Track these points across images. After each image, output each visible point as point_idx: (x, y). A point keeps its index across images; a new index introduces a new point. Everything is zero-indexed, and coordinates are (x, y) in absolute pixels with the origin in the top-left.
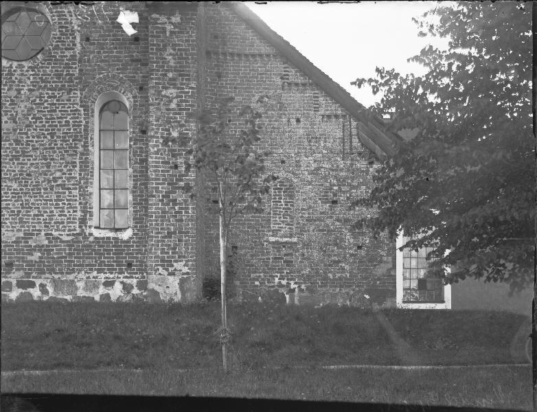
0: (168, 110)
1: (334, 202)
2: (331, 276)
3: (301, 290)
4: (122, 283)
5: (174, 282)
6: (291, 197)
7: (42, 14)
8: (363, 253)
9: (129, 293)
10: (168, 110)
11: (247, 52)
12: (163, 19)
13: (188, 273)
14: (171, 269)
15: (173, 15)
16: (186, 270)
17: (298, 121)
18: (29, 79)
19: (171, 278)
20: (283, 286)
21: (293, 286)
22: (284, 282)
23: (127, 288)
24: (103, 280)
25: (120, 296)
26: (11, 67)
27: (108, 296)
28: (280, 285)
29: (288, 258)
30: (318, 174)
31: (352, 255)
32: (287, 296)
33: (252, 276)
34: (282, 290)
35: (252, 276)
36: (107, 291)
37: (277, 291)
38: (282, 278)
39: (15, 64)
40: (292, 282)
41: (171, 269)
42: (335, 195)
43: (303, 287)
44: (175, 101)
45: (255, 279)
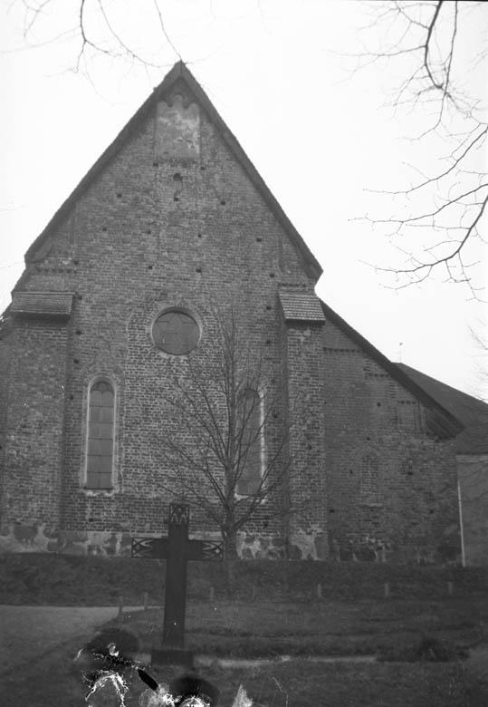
0: (303, 402)
1: (410, 474)
2: (410, 536)
3: (387, 548)
4: (260, 539)
5: (310, 539)
6: (376, 468)
7: (192, 318)
8: (434, 515)
9: (265, 548)
10: (303, 402)
11: (336, 348)
12: (298, 332)
13: (321, 533)
14: (308, 530)
15: (306, 330)
16: (319, 530)
17: (379, 405)
18: (184, 370)
19: (309, 537)
20: (372, 544)
21: (380, 544)
22: (373, 541)
23: (264, 544)
24: (245, 537)
25: (258, 551)
26: (170, 359)
27: (249, 550)
28: (370, 543)
29: (376, 521)
30: (396, 450)
31: (426, 518)
32: (376, 553)
33: (348, 535)
34: (371, 548)
35: (348, 535)
36: (247, 546)
37: (367, 549)
38: (371, 537)
39: (174, 357)
40: (379, 541)
41: (308, 530)
42: (410, 467)
43: (389, 545)
44: (308, 396)
45: (351, 538)
